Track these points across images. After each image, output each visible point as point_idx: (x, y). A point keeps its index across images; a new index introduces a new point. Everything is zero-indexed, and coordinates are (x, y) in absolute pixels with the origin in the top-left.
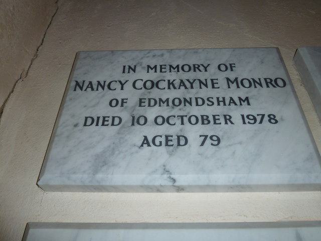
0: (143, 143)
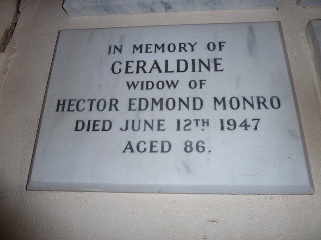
0: (126, 148)
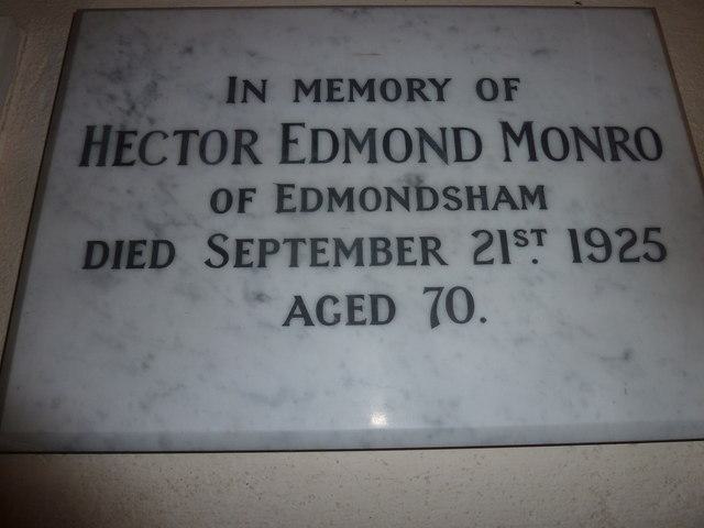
0: (292, 315)
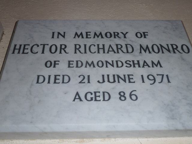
0: (75, 98)
